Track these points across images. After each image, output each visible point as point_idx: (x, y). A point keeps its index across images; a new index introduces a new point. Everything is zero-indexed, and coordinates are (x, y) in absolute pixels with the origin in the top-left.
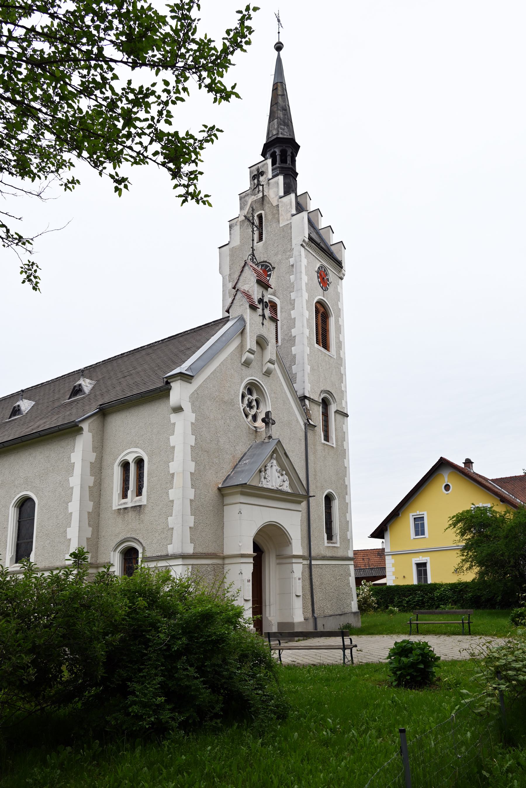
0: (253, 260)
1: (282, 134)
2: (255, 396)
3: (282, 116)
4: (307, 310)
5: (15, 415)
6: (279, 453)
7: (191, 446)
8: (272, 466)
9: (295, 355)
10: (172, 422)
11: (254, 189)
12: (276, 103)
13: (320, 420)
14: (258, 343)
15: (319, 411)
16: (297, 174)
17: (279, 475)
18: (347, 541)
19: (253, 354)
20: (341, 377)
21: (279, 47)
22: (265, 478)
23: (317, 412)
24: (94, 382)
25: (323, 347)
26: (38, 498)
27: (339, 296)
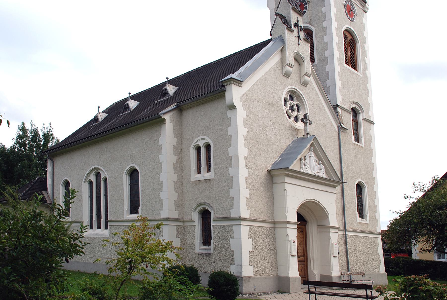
2: (296, 102)
6: (316, 148)
7: (244, 136)
9: (328, 72)
14: (295, 59)
17: (317, 164)
18: (375, 221)
19: (292, 68)
20: (367, 93)
22: (304, 165)
24: (176, 88)
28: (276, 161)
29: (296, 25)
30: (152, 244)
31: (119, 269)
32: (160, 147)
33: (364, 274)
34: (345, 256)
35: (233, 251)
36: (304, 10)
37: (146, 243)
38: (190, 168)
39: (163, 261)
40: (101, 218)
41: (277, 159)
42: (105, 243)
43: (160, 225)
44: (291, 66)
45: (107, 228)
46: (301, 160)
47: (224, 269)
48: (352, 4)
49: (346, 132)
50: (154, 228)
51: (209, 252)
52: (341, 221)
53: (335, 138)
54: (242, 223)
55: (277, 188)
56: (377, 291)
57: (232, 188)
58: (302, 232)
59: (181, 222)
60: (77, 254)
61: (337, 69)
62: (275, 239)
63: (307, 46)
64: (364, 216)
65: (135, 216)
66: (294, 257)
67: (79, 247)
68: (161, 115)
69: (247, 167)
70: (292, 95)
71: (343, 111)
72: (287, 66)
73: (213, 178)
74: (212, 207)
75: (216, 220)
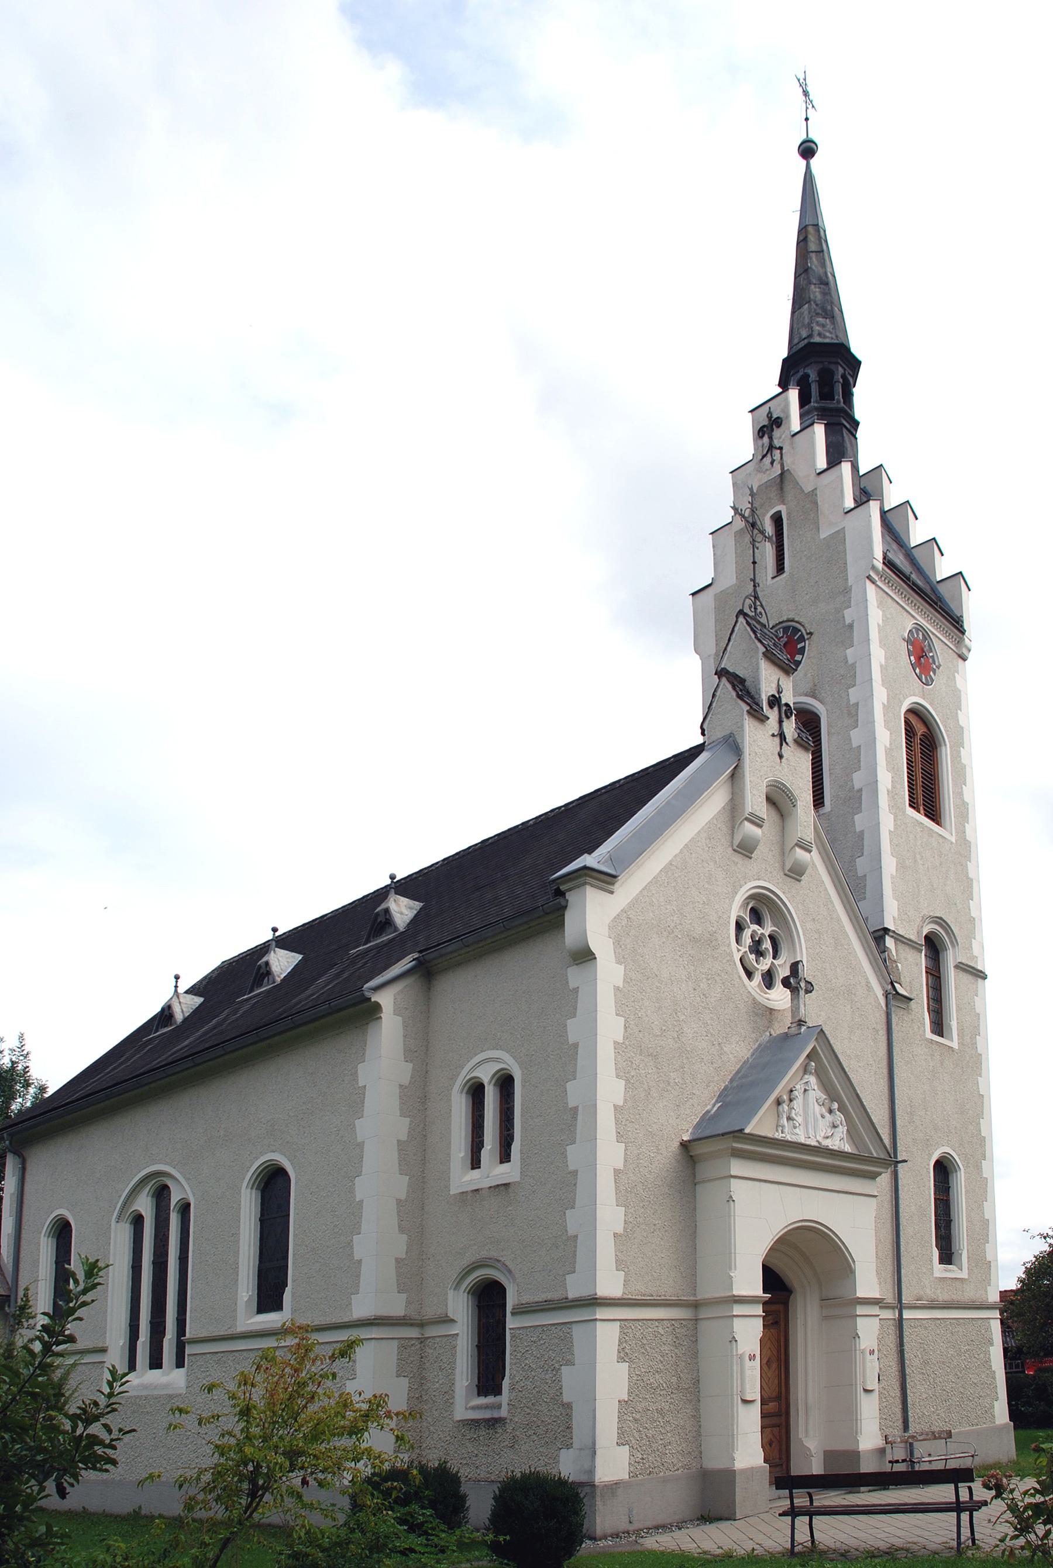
0: (755, 609)
1: (820, 335)
2: (768, 929)
3: (819, 296)
4: (887, 727)
5: (260, 985)
6: (825, 1063)
7: (615, 1042)
8: (805, 1090)
10: (572, 985)
11: (763, 457)
12: (806, 270)
13: (922, 985)
14: (769, 800)
15: (918, 965)
16: (856, 424)
17: (824, 1111)
18: (984, 1267)
19: (760, 826)
20: (968, 887)
21: (807, 150)
22: (789, 1118)
23: (912, 969)
24: (418, 905)
25: (926, 815)
26: (294, 1168)
27: (960, 698)
28: (708, 1112)
29: (774, 701)
30: (324, 1410)
31: (218, 1499)
32: (361, 1093)
33: (949, 1434)
34: (897, 1386)
35: (569, 1406)
36: (798, 658)
37: (305, 1406)
38: (449, 1155)
39: (356, 1460)
40: (163, 1333)
41: (709, 1107)
42: (177, 1418)
43: (351, 1345)
44: (758, 822)
45: (180, 1363)
46: (779, 1102)
47: (541, 1466)
48: (926, 636)
49: (908, 1009)
50: (333, 1358)
51: (496, 1415)
52: (889, 1280)
53: (879, 1027)
54: (601, 1313)
55: (707, 1194)
56: (986, 1486)
57: (573, 1207)
58: (776, 1323)
59: (414, 1326)
60: (94, 1468)
61: (887, 822)
62: (695, 1355)
63: (805, 761)
64: (955, 1258)
65: (271, 1319)
66: (751, 1406)
67: (101, 1443)
68: (366, 993)
69: (620, 1137)
70: (760, 908)
71: (901, 946)
72: (746, 823)
73: (518, 1179)
74: (510, 1271)
75: (521, 1311)
